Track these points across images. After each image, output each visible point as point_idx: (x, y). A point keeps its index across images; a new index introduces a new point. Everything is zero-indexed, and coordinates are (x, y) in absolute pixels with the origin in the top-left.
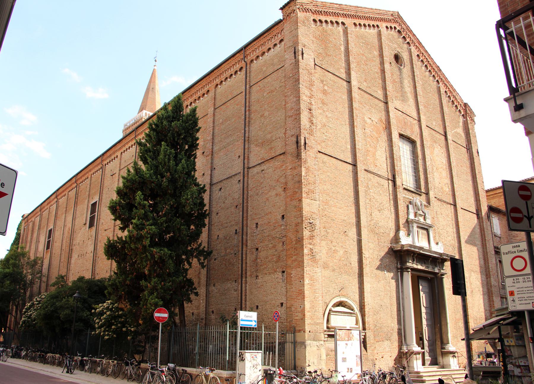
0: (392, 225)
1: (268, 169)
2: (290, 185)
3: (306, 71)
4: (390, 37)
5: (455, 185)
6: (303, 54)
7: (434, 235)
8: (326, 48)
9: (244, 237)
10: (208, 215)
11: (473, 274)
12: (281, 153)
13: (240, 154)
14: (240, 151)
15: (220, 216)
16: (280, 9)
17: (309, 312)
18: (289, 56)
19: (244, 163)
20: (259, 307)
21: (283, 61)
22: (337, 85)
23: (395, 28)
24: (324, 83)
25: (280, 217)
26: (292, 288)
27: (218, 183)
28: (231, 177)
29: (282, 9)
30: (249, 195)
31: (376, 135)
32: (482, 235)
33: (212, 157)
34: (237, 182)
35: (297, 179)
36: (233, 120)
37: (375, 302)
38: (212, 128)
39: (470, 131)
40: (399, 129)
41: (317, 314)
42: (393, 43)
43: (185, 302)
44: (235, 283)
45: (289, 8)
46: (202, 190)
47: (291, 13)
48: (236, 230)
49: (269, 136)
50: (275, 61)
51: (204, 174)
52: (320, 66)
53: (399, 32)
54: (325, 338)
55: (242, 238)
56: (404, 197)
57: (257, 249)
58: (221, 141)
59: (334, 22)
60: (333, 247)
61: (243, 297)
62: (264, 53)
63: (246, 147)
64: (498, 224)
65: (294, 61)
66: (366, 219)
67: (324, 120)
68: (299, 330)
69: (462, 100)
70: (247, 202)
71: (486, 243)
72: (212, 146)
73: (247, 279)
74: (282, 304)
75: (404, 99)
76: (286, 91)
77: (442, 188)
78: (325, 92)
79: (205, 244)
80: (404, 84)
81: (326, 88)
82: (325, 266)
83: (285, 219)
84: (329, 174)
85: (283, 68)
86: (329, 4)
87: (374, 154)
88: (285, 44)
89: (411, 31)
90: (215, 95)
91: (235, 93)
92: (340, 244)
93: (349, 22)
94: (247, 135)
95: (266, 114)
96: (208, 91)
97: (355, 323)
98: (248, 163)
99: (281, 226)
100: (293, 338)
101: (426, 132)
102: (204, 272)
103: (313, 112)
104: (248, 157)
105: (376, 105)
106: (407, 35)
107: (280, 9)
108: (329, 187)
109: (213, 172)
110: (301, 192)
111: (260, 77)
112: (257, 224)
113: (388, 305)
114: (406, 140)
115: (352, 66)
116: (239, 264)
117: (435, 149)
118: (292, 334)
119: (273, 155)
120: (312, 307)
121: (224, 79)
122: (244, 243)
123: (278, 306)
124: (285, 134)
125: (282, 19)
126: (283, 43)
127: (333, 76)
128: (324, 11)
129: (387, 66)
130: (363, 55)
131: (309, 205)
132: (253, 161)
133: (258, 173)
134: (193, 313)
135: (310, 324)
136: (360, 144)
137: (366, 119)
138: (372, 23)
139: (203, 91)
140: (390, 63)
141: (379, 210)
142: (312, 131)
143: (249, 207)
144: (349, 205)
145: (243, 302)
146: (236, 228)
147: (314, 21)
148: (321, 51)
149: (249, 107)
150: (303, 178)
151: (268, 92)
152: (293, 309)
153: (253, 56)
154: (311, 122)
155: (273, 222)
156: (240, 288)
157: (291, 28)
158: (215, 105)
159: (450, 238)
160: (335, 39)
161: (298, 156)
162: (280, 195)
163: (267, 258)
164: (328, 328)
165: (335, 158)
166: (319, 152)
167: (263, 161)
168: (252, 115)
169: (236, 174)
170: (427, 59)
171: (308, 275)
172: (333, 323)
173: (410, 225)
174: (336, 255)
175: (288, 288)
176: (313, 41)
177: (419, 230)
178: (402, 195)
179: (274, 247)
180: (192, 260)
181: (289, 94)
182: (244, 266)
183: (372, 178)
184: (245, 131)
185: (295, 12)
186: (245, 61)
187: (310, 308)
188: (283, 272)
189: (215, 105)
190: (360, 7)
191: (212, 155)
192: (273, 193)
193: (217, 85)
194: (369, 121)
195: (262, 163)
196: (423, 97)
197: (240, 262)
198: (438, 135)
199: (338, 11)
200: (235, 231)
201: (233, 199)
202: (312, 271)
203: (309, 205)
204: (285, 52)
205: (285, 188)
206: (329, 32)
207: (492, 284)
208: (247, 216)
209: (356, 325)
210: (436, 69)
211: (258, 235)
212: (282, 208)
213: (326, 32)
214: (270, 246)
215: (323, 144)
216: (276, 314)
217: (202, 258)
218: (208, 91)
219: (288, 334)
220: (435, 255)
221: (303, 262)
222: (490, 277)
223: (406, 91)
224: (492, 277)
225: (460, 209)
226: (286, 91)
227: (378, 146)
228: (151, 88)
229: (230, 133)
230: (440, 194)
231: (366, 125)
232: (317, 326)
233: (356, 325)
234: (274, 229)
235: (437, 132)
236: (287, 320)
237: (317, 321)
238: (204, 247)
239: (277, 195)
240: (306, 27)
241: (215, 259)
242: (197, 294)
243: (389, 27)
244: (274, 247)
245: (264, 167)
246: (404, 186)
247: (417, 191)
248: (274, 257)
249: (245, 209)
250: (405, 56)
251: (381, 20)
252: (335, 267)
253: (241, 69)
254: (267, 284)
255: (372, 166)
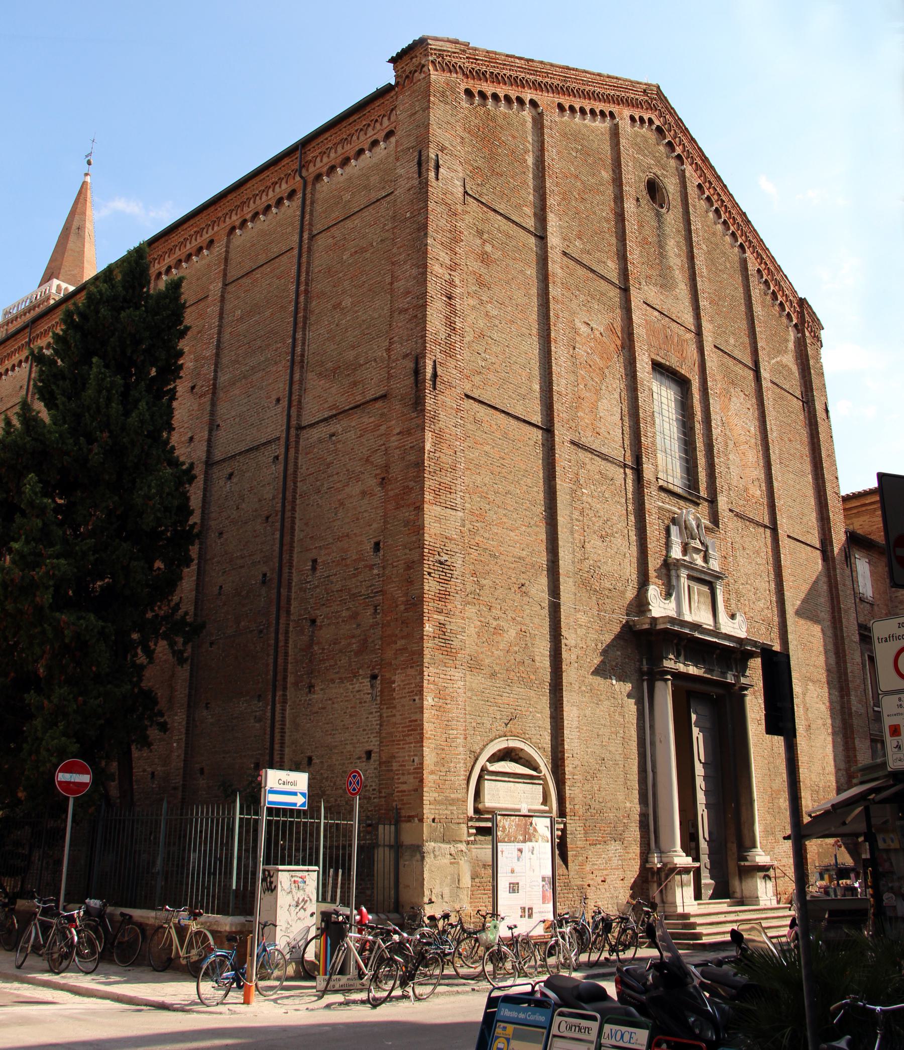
0: (631, 571)
1: (345, 431)
2: (396, 470)
3: (443, 206)
4: (639, 140)
5: (775, 484)
6: (437, 167)
7: (727, 596)
8: (492, 157)
9: (284, 592)
10: (198, 536)
11: (811, 686)
12: (377, 395)
13: (281, 395)
14: (281, 387)
15: (226, 540)
16: (390, 61)
17: (432, 773)
18: (406, 170)
19: (289, 416)
20: (316, 761)
21: (391, 181)
22: (514, 243)
23: (651, 121)
24: (485, 236)
25: (369, 547)
26: (394, 716)
27: (224, 460)
28: (256, 448)
29: (393, 60)
30: (298, 491)
31: (601, 363)
32: (832, 599)
33: (212, 399)
34: (271, 459)
35: (412, 458)
36: (267, 313)
37: (589, 750)
38: (215, 330)
39: (811, 362)
40: (652, 350)
41: (453, 778)
42: (644, 155)
43: (133, 747)
44: (259, 701)
45: (411, 59)
46: (188, 476)
47: (416, 71)
48: (265, 575)
49: (350, 355)
50: (372, 179)
51: (191, 439)
52: (477, 196)
53: (659, 130)
54: (469, 835)
55: (279, 593)
56: (660, 508)
57: (313, 621)
58: (236, 362)
59: (514, 98)
60: (492, 621)
61: (277, 736)
62: (346, 162)
63: (297, 377)
64: (868, 573)
65: (416, 182)
66: (571, 556)
67: (481, 323)
68: (409, 817)
69: (794, 292)
70: (293, 509)
71: (840, 617)
72: (216, 371)
73: (288, 694)
74: (369, 754)
75: (665, 283)
76: (395, 250)
77: (746, 490)
78: (485, 258)
79: (187, 607)
80: (667, 248)
81: (488, 248)
82: (474, 665)
83: (382, 552)
84: (487, 448)
85: (392, 197)
86: (503, 57)
87: (594, 408)
88: (397, 141)
89: (686, 131)
90: (227, 252)
91: (275, 250)
92: (511, 614)
93: (545, 99)
94: (299, 349)
95: (347, 302)
96: (211, 242)
97: (541, 800)
98: (299, 416)
99: (371, 567)
100: (393, 835)
101: (713, 360)
102: (183, 673)
103: (457, 302)
104: (300, 402)
105: (602, 294)
106: (677, 139)
107: (390, 61)
108: (487, 480)
109: (214, 433)
110: (422, 489)
111: (337, 214)
112: (315, 561)
113: (617, 757)
114: (668, 376)
115: (551, 201)
116: (268, 655)
117: (734, 399)
118: (393, 827)
119: (359, 399)
120: (441, 762)
121: (250, 215)
122: (281, 606)
123: (359, 758)
124: (388, 350)
125: (393, 83)
126: (393, 140)
127: (504, 221)
128: (492, 73)
129: (629, 206)
130: (577, 177)
131: (439, 519)
132: (312, 411)
133: (320, 441)
134: (153, 773)
135: (435, 802)
136: (563, 382)
137: (579, 324)
138: (599, 106)
139: (199, 241)
140: (638, 200)
141: (602, 537)
142: (451, 346)
143: (297, 521)
144: (532, 522)
145: (277, 747)
146: (265, 569)
147: (468, 92)
148: (480, 163)
149: (307, 284)
150: (426, 455)
151: (353, 250)
152: (395, 766)
153: (321, 165)
154: (451, 325)
155: (354, 557)
156: (269, 714)
157: (412, 105)
158: (225, 275)
159: (761, 604)
160: (514, 137)
161: (418, 403)
162: (372, 495)
163: (335, 644)
164: (477, 811)
165: (504, 412)
166: (468, 396)
167: (334, 412)
168: (314, 303)
169: (269, 443)
170: (719, 195)
171: (432, 686)
172: (489, 801)
173: (673, 573)
174: (499, 638)
175: (385, 715)
176: (462, 138)
177: (692, 584)
178: (654, 502)
179: (354, 616)
180: (156, 645)
181: (403, 257)
182: (280, 661)
183: (587, 461)
184: (294, 340)
185: (425, 69)
186: (301, 177)
187: (436, 764)
188: (374, 677)
189: (225, 275)
190: (573, 69)
191: (214, 393)
192: (355, 489)
193: (233, 229)
194: (584, 329)
195: (331, 417)
196: (709, 279)
197: (272, 652)
198: (739, 369)
199: (523, 75)
200: (260, 577)
201: (260, 501)
202: (442, 676)
203: (439, 519)
204: (397, 159)
205: (383, 479)
206: (500, 120)
207: (854, 709)
208: (292, 541)
209: (542, 804)
210: (739, 220)
211: (317, 587)
212: (375, 526)
213: (494, 119)
214: (345, 614)
215: (477, 379)
216: (354, 776)
217: (180, 640)
218: (211, 242)
219: (381, 827)
220: (727, 643)
221: (421, 653)
222: (848, 695)
223: (672, 264)
224: (853, 693)
225: (786, 537)
226: (395, 250)
227: (603, 388)
228: (74, 227)
229: (259, 342)
230: (742, 502)
231: (578, 338)
232: (451, 808)
233: (542, 804)
234: (355, 576)
235: (738, 360)
236: (380, 792)
237: (453, 796)
238: (186, 613)
239: (363, 493)
240: (448, 107)
241: (212, 644)
242: (164, 727)
243: (637, 118)
244: (354, 616)
245: (336, 427)
246: (661, 483)
247: (690, 495)
248: (354, 640)
249: (287, 524)
250: (671, 186)
251: (619, 101)
252: (497, 668)
253: (291, 195)
254: (336, 706)
255: (589, 433)
